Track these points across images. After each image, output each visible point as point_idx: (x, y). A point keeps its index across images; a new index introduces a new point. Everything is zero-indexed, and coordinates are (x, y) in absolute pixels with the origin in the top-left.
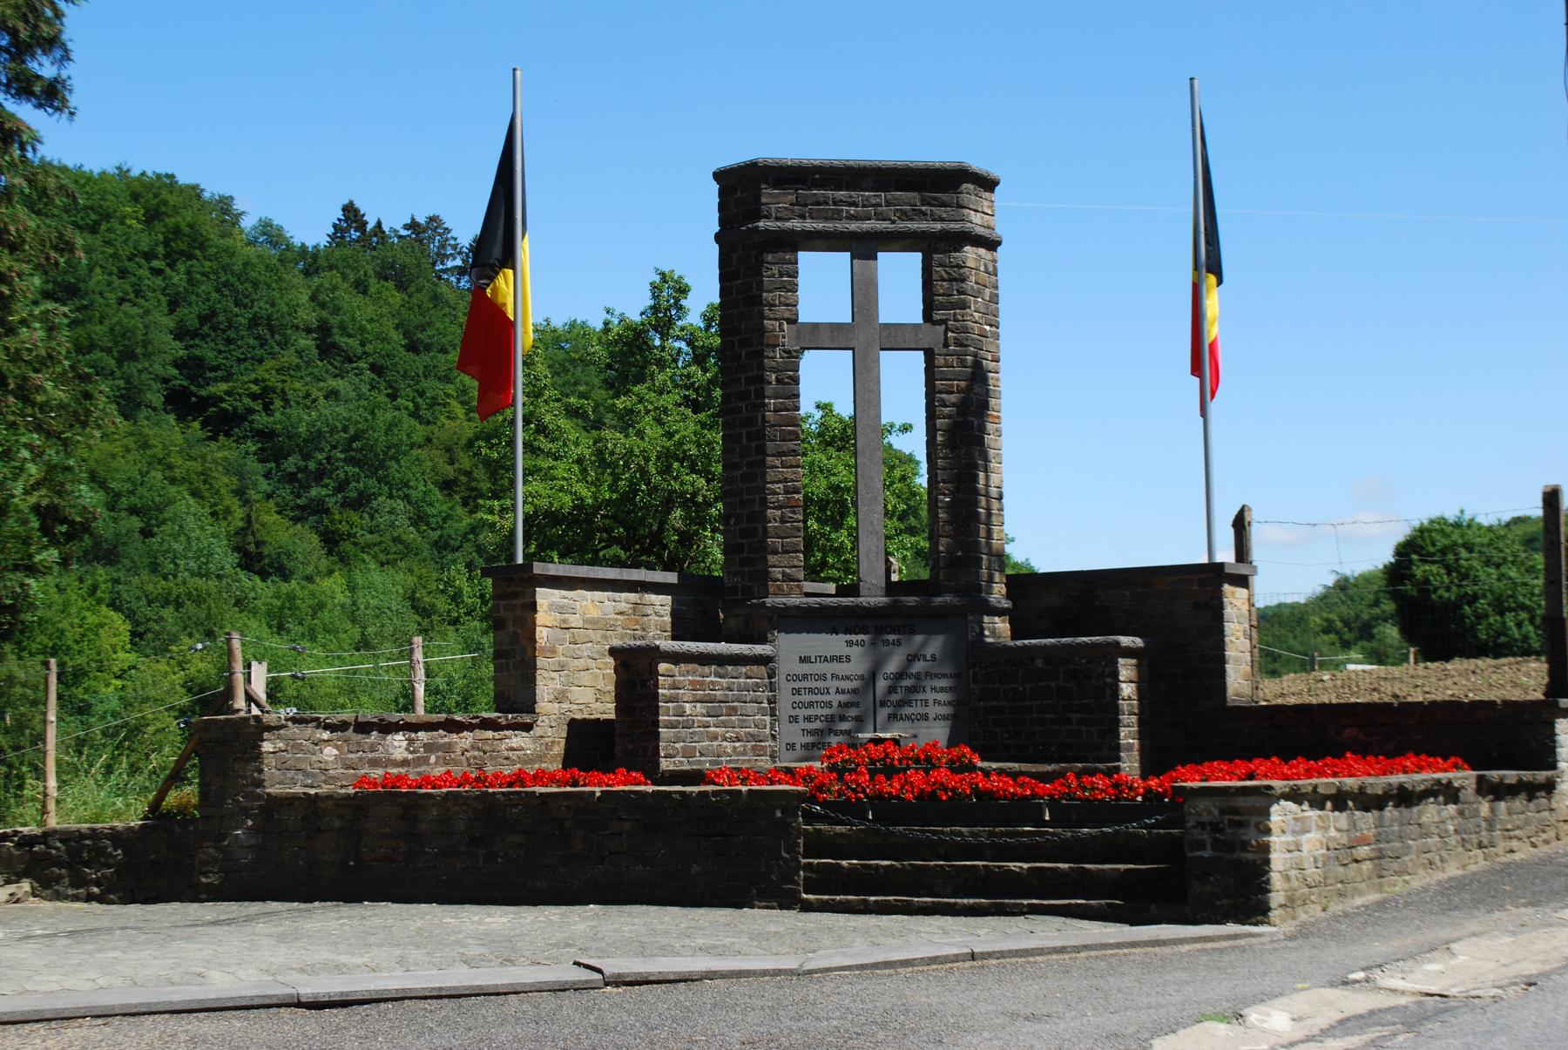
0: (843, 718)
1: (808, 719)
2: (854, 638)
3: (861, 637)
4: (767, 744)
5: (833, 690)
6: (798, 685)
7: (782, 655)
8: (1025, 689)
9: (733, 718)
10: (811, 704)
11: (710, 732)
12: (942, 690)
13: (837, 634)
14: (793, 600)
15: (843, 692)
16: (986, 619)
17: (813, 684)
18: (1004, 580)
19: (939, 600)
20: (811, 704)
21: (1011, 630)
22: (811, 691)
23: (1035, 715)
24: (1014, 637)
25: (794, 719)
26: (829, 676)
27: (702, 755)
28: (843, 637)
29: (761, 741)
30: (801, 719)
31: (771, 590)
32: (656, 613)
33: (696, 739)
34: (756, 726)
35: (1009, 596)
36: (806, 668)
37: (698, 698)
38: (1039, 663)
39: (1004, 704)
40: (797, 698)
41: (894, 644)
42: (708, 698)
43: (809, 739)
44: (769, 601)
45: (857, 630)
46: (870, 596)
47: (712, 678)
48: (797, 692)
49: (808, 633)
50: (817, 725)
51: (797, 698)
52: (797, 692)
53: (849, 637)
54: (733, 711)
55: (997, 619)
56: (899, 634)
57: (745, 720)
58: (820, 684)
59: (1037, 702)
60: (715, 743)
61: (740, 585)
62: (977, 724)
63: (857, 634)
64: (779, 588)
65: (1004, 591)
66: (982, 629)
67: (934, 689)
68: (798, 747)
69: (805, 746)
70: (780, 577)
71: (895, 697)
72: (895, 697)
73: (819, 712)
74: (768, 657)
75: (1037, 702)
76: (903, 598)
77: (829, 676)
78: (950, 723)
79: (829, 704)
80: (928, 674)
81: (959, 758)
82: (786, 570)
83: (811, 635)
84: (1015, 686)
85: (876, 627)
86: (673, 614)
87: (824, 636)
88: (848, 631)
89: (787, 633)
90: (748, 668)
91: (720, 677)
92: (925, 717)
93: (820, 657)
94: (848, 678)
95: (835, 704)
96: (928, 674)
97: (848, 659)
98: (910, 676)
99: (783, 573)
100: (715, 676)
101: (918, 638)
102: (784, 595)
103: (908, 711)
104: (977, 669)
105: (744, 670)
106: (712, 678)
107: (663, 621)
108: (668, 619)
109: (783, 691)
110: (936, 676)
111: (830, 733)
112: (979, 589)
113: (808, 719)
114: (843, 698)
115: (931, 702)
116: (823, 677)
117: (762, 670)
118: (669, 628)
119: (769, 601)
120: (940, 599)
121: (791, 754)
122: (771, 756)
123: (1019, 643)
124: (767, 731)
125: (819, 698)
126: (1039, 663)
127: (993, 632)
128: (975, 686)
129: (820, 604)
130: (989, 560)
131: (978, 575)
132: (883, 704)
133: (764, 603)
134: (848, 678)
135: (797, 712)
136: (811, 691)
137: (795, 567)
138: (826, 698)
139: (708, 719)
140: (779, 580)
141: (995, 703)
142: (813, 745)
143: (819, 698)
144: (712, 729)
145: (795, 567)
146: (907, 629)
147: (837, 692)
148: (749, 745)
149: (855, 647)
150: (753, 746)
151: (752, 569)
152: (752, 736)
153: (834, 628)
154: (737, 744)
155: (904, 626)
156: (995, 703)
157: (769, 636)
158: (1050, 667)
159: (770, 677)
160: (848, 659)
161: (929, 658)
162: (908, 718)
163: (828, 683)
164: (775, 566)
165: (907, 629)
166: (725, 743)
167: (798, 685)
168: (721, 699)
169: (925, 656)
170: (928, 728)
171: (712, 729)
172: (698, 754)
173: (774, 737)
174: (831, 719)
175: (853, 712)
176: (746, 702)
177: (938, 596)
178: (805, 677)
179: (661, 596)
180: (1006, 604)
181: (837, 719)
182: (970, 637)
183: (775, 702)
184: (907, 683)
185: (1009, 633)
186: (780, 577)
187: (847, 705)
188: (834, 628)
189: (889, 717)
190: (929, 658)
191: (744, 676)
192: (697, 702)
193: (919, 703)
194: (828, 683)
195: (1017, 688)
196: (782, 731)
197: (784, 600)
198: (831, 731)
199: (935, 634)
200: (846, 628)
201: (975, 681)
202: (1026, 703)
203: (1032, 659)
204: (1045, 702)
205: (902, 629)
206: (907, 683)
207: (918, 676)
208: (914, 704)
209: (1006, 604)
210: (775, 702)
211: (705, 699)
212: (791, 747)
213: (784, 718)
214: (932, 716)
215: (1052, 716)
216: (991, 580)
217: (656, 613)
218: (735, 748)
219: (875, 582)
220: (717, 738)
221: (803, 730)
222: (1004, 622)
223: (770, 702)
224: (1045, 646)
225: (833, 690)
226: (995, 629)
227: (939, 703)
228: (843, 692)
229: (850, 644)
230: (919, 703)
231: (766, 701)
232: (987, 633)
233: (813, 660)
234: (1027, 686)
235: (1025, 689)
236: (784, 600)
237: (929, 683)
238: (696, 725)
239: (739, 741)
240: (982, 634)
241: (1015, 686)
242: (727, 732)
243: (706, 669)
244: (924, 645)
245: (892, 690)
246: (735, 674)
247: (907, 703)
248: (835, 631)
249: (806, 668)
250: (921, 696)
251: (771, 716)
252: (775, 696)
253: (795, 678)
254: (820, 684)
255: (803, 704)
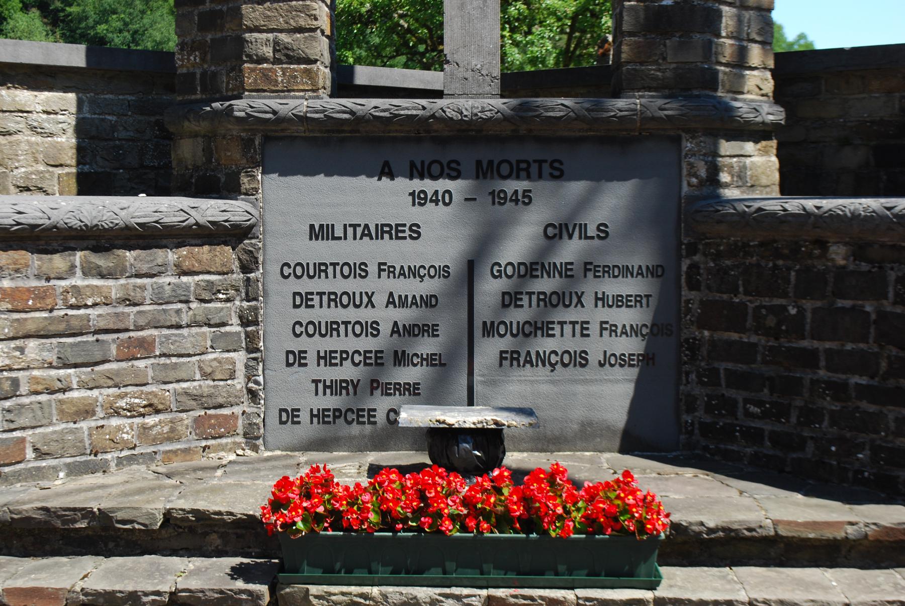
0: (401, 359)
1: (327, 358)
2: (429, 186)
3: (443, 184)
4: (237, 410)
5: (380, 299)
6: (305, 285)
7: (273, 222)
8: (801, 311)
9: (141, 364)
10: (333, 328)
11: (71, 401)
12: (620, 301)
13: (392, 177)
14: (292, 103)
15: (403, 302)
16: (726, 147)
17: (338, 285)
18: (771, 64)
19: (621, 104)
20: (333, 328)
21: (781, 171)
22: (334, 299)
23: (822, 373)
24: (788, 187)
25: (297, 359)
26: (373, 269)
27: (41, 454)
28: (404, 185)
29: (221, 406)
30: (311, 358)
31: (249, 81)
32: (33, 129)
33: (22, 421)
34: (206, 376)
35: (779, 97)
36: (324, 251)
37: (31, 327)
38: (838, 254)
39: (754, 339)
40: (304, 315)
41: (516, 201)
42: (62, 327)
43: (330, 402)
44: (240, 106)
45: (436, 169)
46: (464, 95)
47: (78, 281)
48: (303, 300)
49: (329, 174)
50: (347, 372)
51: (304, 315)
52: (303, 300)
53: (417, 185)
54: (145, 348)
55: (749, 147)
56: (529, 177)
57: (175, 366)
58: (354, 285)
59: (828, 345)
60: (84, 425)
61: (198, 72)
62: (693, 376)
63: (435, 178)
64: (266, 76)
65: (769, 86)
66: (714, 170)
67: (600, 299)
68: (304, 417)
69: (319, 416)
70: (268, 52)
71: (517, 316)
72: (517, 316)
73: (350, 343)
74: (236, 226)
75: (828, 345)
76: (540, 100)
77: (373, 269)
78: (633, 373)
79: (373, 329)
80: (588, 267)
81: (613, 519)
82: (284, 37)
83: (336, 179)
84: (783, 301)
85: (479, 163)
86: (81, 129)
87: (363, 180)
88: (417, 171)
89: (283, 173)
90: (184, 251)
91: (103, 277)
92: (580, 360)
93: (355, 226)
94: (414, 273)
95: (385, 328)
96: (588, 267)
97: (415, 232)
98: (549, 270)
99: (276, 43)
100: (86, 274)
101: (576, 188)
102: (277, 92)
103: (545, 345)
104: (697, 258)
105: (171, 256)
106: (78, 281)
107: (54, 146)
108: (67, 141)
109: (273, 298)
110: (608, 271)
111: (372, 390)
112: (712, 81)
113: (327, 358)
114: (404, 316)
115: (594, 329)
116: (360, 270)
117: (227, 255)
118: (70, 157)
119: (240, 106)
120: (621, 103)
121: (291, 433)
122: (245, 435)
123: (794, 205)
124: (239, 383)
125: (351, 314)
126: (838, 254)
127: (741, 176)
128: (693, 294)
129: (352, 113)
130: (739, 20)
131: (709, 51)
132: (490, 330)
133: (230, 108)
134: (414, 273)
135: (304, 343)
136: (334, 299)
137: (300, 30)
138: (365, 315)
139: (62, 372)
140: (264, 60)
141: (735, 336)
142: (337, 413)
143: (351, 314)
144: (75, 394)
145: (300, 30)
146: (546, 168)
147: (391, 302)
148: (187, 418)
149: (430, 206)
150: (197, 420)
151: (219, 35)
152: (195, 397)
153: (386, 164)
154: (150, 420)
155: (540, 162)
156: (735, 336)
157: (244, 180)
158: (864, 267)
159: (246, 269)
160: (415, 232)
161: (592, 231)
162: (543, 360)
163: (371, 284)
164: (257, 29)
165: (546, 168)
166: (115, 422)
167: (305, 285)
168: (102, 324)
169: (583, 228)
170: (585, 382)
171: (75, 394)
172: (30, 454)
173: (253, 395)
174: (375, 359)
175: (426, 346)
176: (179, 327)
177: (617, 95)
178: (321, 269)
179: (47, 94)
180: (772, 114)
181: (389, 359)
182: (685, 188)
183: (256, 323)
184: (545, 285)
185: (776, 176)
186: (268, 52)
187: (412, 331)
188: (386, 164)
189: (502, 359)
190: (592, 231)
191: (172, 269)
192: (28, 336)
193: (568, 329)
194: (371, 284)
195: (784, 308)
196: (270, 384)
197: (274, 103)
198: (374, 385)
199: (610, 179)
200: (413, 165)
201: (693, 285)
202: (805, 344)
203: (822, 244)
204: (849, 347)
205: (534, 169)
206: (545, 285)
207: (566, 271)
208: (557, 331)
209: (772, 114)
210: (256, 323)
211: (53, 328)
212: (290, 416)
213: (277, 358)
214: (594, 357)
215: (863, 381)
216: (741, 63)
217: (33, 129)
218: (145, 428)
219: (476, 63)
220: (94, 413)
221: (316, 382)
222: (765, 152)
223: (245, 322)
224: (855, 217)
225: (380, 299)
226: (744, 168)
227: (613, 329)
228: (403, 302)
229: (419, 198)
230: (568, 329)
231: (235, 320)
232: (725, 177)
233: (339, 232)
234: (809, 305)
235: (801, 311)
236: (274, 103)
237: (590, 287)
238: (24, 389)
239: (158, 412)
240: (713, 180)
241: (783, 301)
242: (121, 397)
243: (58, 261)
244: (585, 202)
245: (510, 299)
246: (144, 268)
247: (539, 328)
248: (387, 171)
249: (324, 251)
250: (572, 314)
251: (249, 350)
252: (256, 309)
253: (302, 270)
254: (354, 285)
255: (317, 326)
